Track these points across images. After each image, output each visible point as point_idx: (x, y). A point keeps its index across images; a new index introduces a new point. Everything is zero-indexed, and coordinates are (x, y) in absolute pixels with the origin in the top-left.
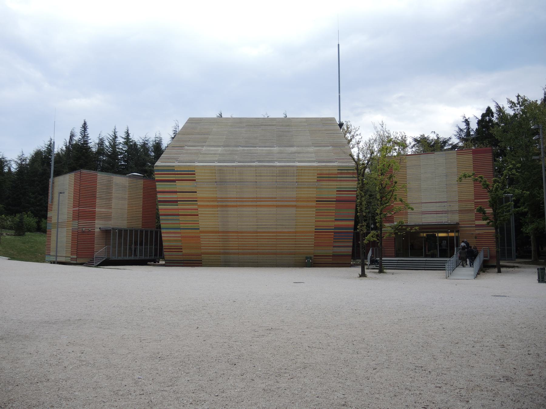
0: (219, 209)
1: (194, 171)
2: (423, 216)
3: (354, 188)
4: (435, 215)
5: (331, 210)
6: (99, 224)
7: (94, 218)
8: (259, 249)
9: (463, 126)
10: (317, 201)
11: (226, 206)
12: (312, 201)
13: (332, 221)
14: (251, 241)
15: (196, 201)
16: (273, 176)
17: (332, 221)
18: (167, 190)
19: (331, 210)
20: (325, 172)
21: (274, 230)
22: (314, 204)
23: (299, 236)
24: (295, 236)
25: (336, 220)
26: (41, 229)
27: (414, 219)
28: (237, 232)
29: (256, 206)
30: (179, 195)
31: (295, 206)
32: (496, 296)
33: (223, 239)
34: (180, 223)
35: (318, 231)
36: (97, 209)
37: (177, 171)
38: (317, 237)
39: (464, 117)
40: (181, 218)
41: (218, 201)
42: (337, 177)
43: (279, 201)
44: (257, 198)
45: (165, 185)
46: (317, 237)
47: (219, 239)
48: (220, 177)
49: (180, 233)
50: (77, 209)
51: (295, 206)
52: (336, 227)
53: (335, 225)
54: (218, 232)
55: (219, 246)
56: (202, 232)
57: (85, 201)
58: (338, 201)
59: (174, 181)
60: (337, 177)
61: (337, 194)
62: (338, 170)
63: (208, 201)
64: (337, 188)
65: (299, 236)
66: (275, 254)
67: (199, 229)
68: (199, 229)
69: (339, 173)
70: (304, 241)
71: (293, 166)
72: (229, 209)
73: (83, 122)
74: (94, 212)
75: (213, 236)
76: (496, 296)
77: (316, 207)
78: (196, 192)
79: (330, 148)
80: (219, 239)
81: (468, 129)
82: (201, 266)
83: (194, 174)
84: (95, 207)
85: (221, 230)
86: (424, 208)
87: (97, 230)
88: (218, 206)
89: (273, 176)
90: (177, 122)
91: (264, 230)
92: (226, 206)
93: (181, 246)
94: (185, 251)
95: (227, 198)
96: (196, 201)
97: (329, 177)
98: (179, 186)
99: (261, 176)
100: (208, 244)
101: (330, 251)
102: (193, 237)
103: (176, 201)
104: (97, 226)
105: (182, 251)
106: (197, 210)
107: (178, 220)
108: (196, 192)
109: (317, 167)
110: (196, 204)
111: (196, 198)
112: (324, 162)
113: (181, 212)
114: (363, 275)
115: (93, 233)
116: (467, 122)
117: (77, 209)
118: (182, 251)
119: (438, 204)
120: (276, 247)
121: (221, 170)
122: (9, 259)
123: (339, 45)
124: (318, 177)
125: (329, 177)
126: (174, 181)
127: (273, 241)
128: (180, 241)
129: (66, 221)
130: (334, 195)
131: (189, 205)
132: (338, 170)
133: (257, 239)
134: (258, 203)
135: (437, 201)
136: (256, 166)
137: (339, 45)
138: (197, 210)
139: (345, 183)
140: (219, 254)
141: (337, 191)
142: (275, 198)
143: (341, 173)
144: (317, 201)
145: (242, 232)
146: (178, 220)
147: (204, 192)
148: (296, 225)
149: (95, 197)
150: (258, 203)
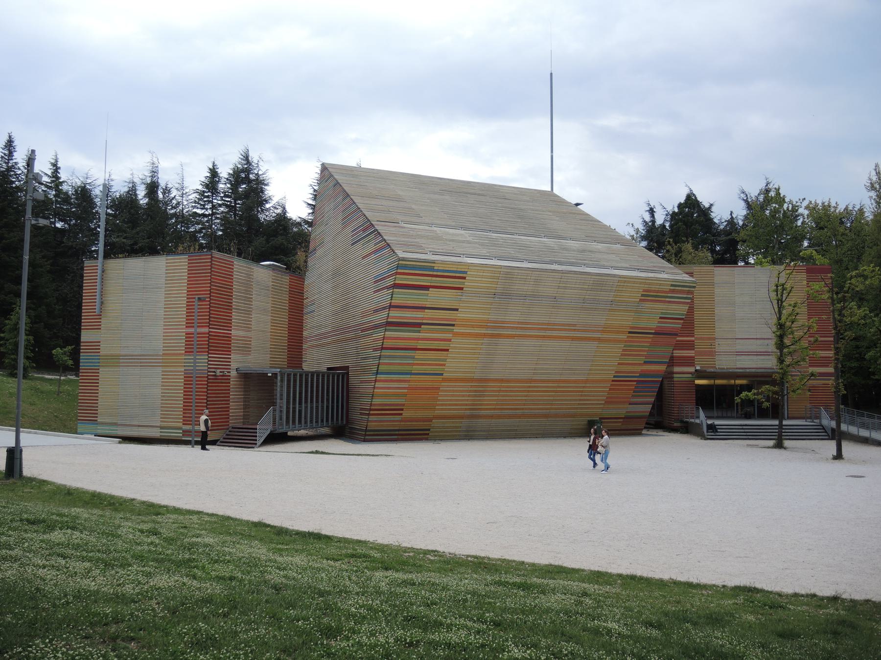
0: (486, 340)
1: (465, 272)
2: (738, 358)
3: (682, 315)
4: (755, 358)
5: (642, 346)
6: (237, 362)
7: (228, 351)
8: (526, 409)
9: (648, 218)
10: (630, 332)
11: (499, 336)
12: (623, 332)
13: (640, 364)
14: (518, 396)
15: (453, 325)
16: (582, 289)
17: (640, 364)
18: (409, 303)
19: (642, 346)
20: (653, 287)
21: (558, 378)
22: (624, 337)
23: (589, 387)
24: (584, 387)
25: (646, 363)
26: (75, 368)
27: (725, 362)
28: (502, 381)
29: (544, 337)
30: (428, 314)
31: (599, 340)
32: (855, 477)
33: (476, 391)
34: (414, 364)
35: (618, 380)
36: (233, 332)
37: (438, 271)
38: (613, 389)
39: (649, 205)
40: (418, 354)
41: (487, 327)
42: (667, 297)
43: (578, 330)
44: (548, 324)
45: (404, 294)
46: (613, 389)
47: (470, 391)
48: (504, 287)
49: (408, 381)
50: (206, 330)
51: (599, 340)
52: (643, 374)
53: (642, 371)
54: (472, 380)
55: (466, 405)
56: (445, 380)
57: (211, 316)
58: (658, 333)
59: (426, 288)
60: (667, 297)
61: (659, 322)
62: (672, 285)
63: (473, 326)
64: (662, 313)
65: (589, 387)
66: (546, 416)
67: (442, 374)
68: (442, 374)
69: (673, 291)
70: (594, 396)
71: (614, 276)
72: (502, 341)
73: (6, 138)
74: (229, 337)
75: (463, 387)
76: (855, 477)
77: (626, 341)
78: (457, 310)
79: (618, 246)
80: (470, 391)
81: (653, 222)
82: (427, 439)
83: (464, 278)
84: (229, 328)
85: (477, 376)
86: (741, 346)
87: (233, 373)
88: (484, 335)
89: (582, 289)
90: (155, 160)
91: (544, 377)
92: (499, 336)
93: (403, 405)
94: (406, 414)
95: (503, 322)
96: (453, 325)
97: (656, 296)
98: (434, 297)
99: (565, 288)
100: (451, 400)
101: (622, 410)
102: (427, 389)
103: (419, 325)
104: (234, 365)
105: (401, 414)
106: (450, 340)
107: (413, 358)
108: (457, 310)
109: (646, 279)
110: (452, 332)
111: (455, 320)
112: (652, 271)
113: (421, 344)
114: (839, 456)
115: (226, 379)
116: (652, 211)
117: (206, 330)
118: (401, 414)
119: (759, 342)
120: (552, 404)
121: (509, 273)
122: (120, 443)
123: (551, 74)
124: (643, 295)
125: (656, 296)
126: (426, 288)
127: (549, 396)
128: (405, 395)
129: (161, 353)
130: (653, 323)
131: (437, 331)
132: (672, 285)
133: (528, 391)
134: (548, 333)
135: (758, 336)
136: (562, 272)
137: (551, 74)
138: (450, 340)
139: (674, 306)
140: (462, 417)
141: (661, 318)
142: (575, 325)
143: (673, 291)
144: (630, 332)
145: (508, 381)
146: (413, 358)
147: (471, 309)
148: (590, 370)
149: (229, 307)
150: (548, 333)
